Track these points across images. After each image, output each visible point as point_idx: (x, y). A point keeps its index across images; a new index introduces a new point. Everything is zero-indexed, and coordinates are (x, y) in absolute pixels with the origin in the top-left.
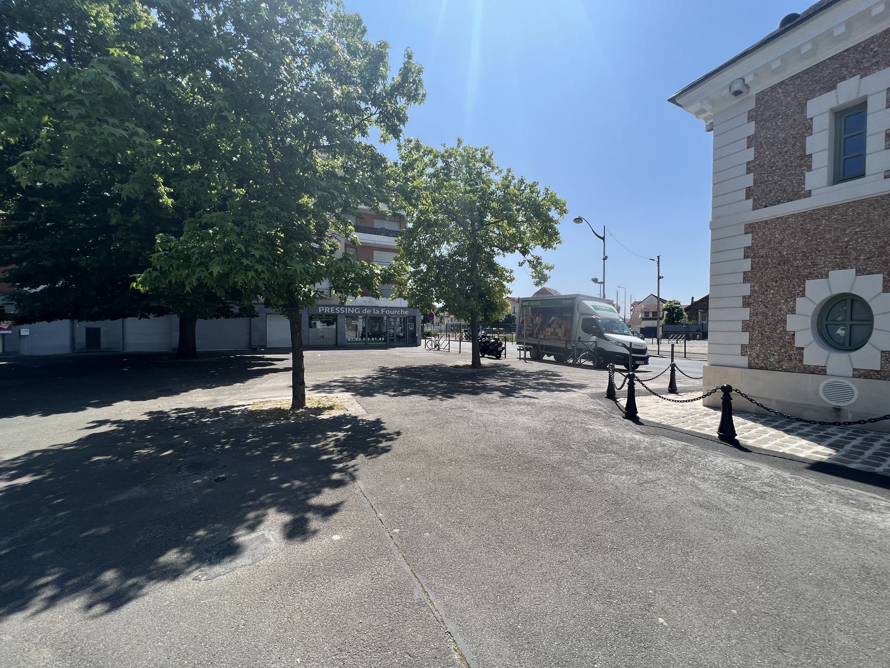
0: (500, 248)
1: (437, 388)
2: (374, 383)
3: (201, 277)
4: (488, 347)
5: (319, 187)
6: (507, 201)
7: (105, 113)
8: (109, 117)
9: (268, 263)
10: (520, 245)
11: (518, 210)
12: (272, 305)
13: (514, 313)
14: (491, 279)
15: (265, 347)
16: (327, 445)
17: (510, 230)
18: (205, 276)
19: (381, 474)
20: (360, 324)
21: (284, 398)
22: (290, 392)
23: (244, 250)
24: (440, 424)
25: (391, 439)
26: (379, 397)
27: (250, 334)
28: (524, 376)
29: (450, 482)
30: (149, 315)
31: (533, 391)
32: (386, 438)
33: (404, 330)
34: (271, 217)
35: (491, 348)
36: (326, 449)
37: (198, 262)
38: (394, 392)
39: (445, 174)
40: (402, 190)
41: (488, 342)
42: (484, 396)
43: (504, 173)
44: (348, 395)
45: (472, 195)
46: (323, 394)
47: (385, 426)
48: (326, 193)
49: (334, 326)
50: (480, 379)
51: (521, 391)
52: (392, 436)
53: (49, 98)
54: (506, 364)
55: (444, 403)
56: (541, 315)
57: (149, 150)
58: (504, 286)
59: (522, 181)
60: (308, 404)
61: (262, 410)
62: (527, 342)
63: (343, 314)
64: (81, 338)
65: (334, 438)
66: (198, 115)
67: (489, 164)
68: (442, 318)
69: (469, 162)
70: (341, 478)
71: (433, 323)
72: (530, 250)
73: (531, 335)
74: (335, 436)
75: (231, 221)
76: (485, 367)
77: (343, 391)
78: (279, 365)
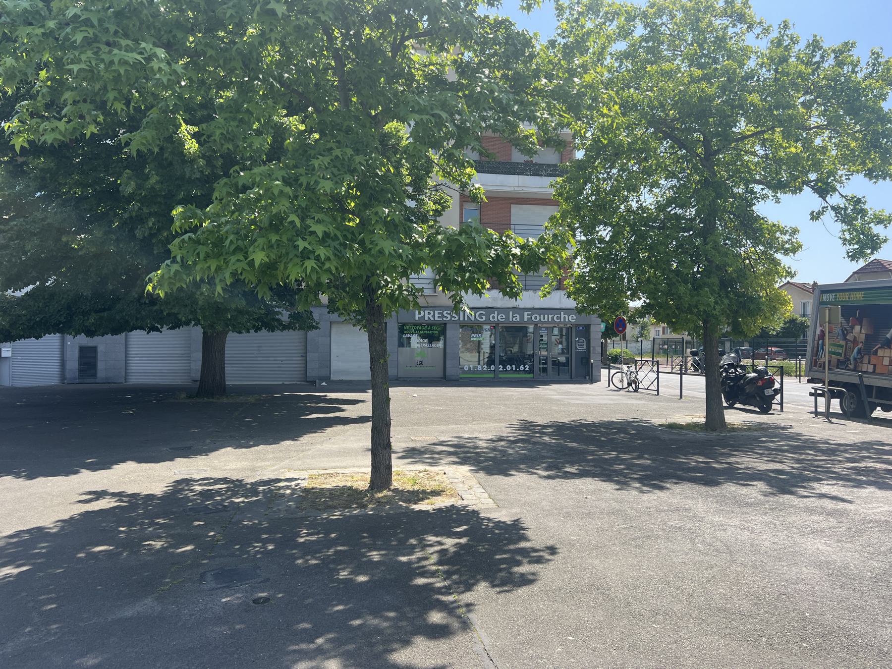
0: (769, 185)
1: (630, 466)
2: (511, 451)
3: (236, 270)
4: (741, 389)
5: (416, 108)
6: (783, 88)
7: (116, 32)
8: (121, 38)
9: (336, 244)
10: (813, 176)
11: (807, 105)
12: (338, 309)
13: (804, 316)
14: (747, 248)
15: (327, 379)
16: (426, 559)
17: (790, 146)
18: (243, 269)
19: (520, 622)
20: (486, 339)
21: (357, 470)
22: (368, 460)
23: (298, 225)
24: (635, 540)
25: (539, 560)
26: (519, 479)
27: (305, 356)
28: (823, 452)
29: (653, 655)
30: (162, 327)
31: (844, 486)
32: (530, 557)
33: (567, 351)
34: (340, 166)
35: (748, 389)
36: (423, 567)
37: (233, 247)
38: (546, 469)
39: (649, 50)
40: (560, 94)
41: (743, 377)
42: (731, 488)
43: (774, 34)
44: (465, 470)
45: (704, 85)
46: (421, 467)
47: (528, 533)
48: (427, 117)
49: (440, 344)
50: (722, 454)
51: (815, 485)
52: (541, 554)
53: (51, 24)
54: (783, 424)
55: (645, 497)
56: (865, 321)
57: (170, 77)
58: (776, 263)
59: (815, 45)
60: (396, 484)
61: (322, 489)
62: (833, 378)
63: (455, 322)
64: (73, 363)
65: (438, 548)
66: (234, 14)
67: (741, 18)
68: (643, 327)
69: (698, 20)
70: (444, 622)
71: (624, 338)
72: (838, 186)
73: (842, 364)
74: (440, 543)
75: (281, 179)
76: (734, 429)
77: (454, 463)
78: (351, 411)
